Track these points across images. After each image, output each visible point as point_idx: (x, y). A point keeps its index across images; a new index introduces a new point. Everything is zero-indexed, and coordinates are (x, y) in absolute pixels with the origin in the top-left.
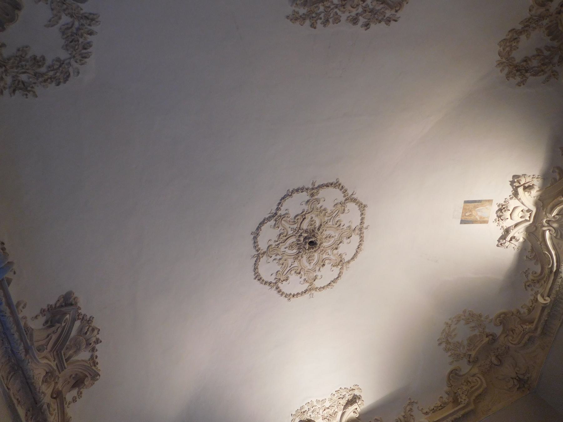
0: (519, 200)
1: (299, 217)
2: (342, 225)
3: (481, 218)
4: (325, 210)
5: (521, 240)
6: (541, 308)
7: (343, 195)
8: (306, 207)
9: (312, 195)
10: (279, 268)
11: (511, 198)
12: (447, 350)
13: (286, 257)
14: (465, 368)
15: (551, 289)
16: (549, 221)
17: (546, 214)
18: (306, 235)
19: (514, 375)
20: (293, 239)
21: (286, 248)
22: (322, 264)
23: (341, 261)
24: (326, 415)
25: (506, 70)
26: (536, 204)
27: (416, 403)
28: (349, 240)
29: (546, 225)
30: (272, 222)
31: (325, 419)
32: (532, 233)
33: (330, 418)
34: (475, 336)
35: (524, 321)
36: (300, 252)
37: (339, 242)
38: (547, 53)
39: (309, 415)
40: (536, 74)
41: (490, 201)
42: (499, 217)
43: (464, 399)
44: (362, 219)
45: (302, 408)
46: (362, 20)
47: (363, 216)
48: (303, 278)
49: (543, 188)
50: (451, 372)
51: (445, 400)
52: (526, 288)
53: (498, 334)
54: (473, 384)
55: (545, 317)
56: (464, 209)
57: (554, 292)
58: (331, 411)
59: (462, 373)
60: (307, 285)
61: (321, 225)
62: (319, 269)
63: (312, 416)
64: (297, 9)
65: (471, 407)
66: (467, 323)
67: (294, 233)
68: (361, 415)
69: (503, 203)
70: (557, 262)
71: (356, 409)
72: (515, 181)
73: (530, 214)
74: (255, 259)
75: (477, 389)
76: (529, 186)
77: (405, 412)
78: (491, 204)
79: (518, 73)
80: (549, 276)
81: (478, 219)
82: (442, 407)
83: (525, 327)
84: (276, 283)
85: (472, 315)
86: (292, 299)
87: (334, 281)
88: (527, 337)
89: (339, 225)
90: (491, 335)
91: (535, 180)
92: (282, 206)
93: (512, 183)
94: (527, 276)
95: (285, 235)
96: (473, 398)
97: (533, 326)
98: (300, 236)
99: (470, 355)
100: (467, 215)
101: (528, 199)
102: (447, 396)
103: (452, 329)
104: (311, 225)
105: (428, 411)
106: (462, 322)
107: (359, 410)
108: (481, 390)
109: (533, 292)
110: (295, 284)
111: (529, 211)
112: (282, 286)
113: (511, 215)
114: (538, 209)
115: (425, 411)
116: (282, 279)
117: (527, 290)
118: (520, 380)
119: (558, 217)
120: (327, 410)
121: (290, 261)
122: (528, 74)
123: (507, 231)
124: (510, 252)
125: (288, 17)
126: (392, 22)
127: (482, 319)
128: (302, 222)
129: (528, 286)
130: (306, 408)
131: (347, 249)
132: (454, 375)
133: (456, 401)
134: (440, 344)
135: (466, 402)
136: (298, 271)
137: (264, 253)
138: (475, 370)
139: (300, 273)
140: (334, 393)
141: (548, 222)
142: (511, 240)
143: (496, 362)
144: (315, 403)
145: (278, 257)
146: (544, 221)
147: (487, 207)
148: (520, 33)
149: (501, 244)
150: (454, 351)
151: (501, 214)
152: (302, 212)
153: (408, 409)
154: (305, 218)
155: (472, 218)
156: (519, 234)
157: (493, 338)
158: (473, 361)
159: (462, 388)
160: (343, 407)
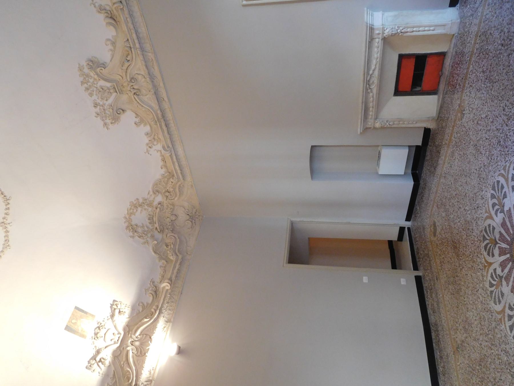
0: (113, 321)
3: (82, 330)
5: (107, 363)
7: (4, 216)
25: (126, 224)
26: (124, 330)
32: (117, 357)
38: (146, 229)
40: (140, 237)
41: (93, 316)
42: (96, 334)
46: (97, 110)
56: (73, 314)
64: (85, 66)
65: (180, 257)
72: (114, 305)
79: (131, 230)
81: (80, 331)
93: (112, 305)
101: (122, 320)
111: (119, 333)
123: (98, 352)
125: (79, 64)
142: (100, 361)
146: (129, 341)
148: (140, 205)
149: (90, 366)
156: (107, 355)
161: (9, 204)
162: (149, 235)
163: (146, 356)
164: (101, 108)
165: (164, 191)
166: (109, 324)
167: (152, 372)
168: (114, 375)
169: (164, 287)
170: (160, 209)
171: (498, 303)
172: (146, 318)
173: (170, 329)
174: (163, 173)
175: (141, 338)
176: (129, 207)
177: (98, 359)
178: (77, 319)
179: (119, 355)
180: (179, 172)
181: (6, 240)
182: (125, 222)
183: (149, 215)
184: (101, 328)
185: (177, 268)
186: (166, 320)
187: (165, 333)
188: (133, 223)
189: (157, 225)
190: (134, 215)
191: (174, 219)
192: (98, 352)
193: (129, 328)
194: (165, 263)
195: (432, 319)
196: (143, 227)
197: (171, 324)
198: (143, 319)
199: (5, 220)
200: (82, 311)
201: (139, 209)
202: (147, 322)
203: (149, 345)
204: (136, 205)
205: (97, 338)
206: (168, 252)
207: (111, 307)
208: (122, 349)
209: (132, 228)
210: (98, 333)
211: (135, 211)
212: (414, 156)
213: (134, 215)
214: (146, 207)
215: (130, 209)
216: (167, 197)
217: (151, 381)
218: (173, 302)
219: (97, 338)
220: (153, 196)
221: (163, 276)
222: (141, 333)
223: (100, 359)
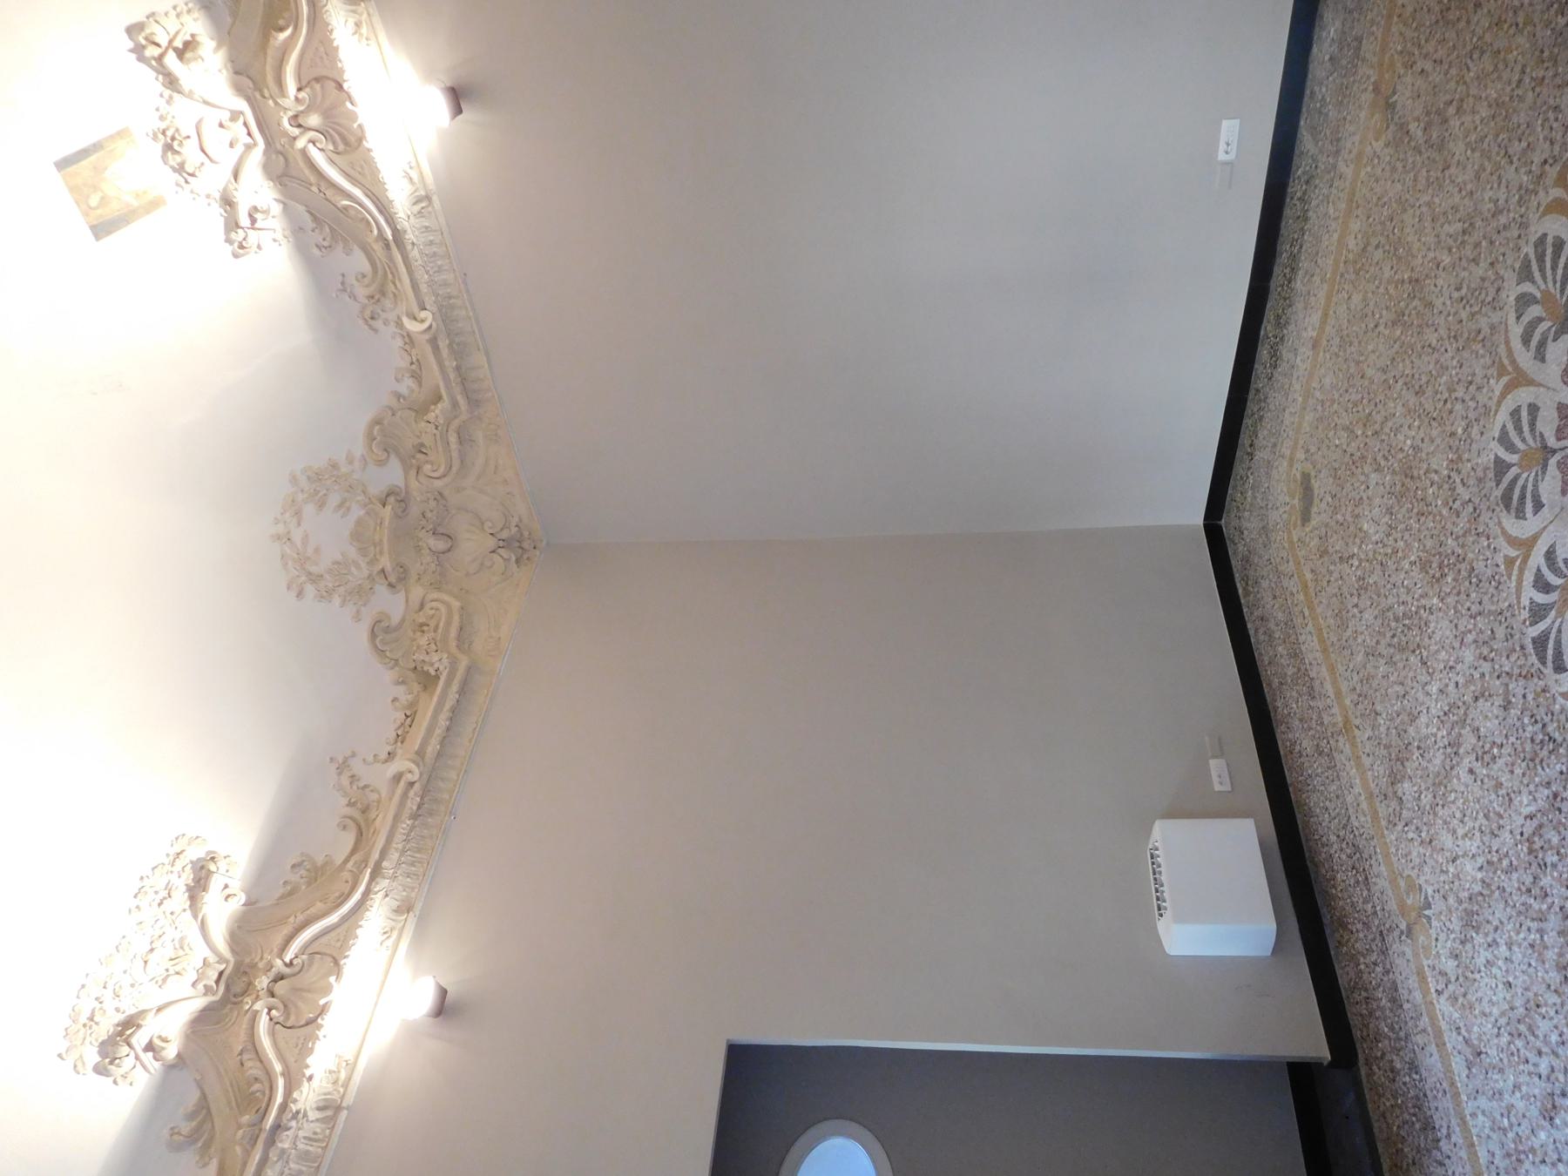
0: (190, 95)
11: (169, 101)
12: (326, 595)
14: (393, 605)
15: (415, 286)
16: (296, 116)
17: (276, 103)
19: (491, 543)
26: (239, 90)
27: (354, 755)
29: (296, 131)
31: (164, 980)
33: (177, 968)
34: (359, 522)
35: (421, 410)
41: (121, 134)
42: (180, 169)
43: (438, 662)
49: (227, 36)
50: (373, 635)
51: (405, 698)
52: (371, 327)
53: (401, 483)
54: (432, 624)
55: (450, 364)
56: (72, 189)
57: (424, 288)
58: (165, 952)
59: (395, 620)
65: (464, 662)
66: (321, 505)
68: (248, 892)
70: (381, 212)
71: (226, 886)
73: (245, 124)
75: (448, 623)
77: (345, 794)
80: (391, 258)
81: (135, 203)
82: (410, 717)
83: (431, 416)
85: (316, 477)
88: (453, 439)
91: (186, 18)
93: (138, 50)
94: (353, 296)
96: (453, 644)
97: (445, 404)
99: (383, 571)
101: (209, 72)
102: (402, 688)
103: (298, 543)
105: (389, 748)
106: (309, 509)
108: (456, 618)
109: (392, 328)
111: (235, 116)
114: (249, 100)
115: (384, 756)
117: (376, 331)
118: (506, 543)
119: (302, 95)
123: (228, 202)
124: (273, 267)
127: (344, 470)
132: (381, 633)
133: (428, 681)
134: (300, 595)
135: (445, 661)
138: (417, 592)
142: (253, 221)
143: (441, 545)
149: (241, 247)
150: (342, 589)
151: (178, 159)
153: (345, 781)
156: (257, 191)
157: (397, 498)
158: (398, 579)
159: (419, 647)
168: (315, 219)
171: (1550, 240)
172: (281, 29)
173: (376, 19)
175: (313, 98)
177: (244, 221)
178: (95, 188)
179: (286, 170)
184: (176, 147)
187: (373, 42)
192: (228, 202)
193: (252, 77)
195: (1306, 142)
200: (83, 154)
202: (292, 41)
205: (192, 175)
207: (142, 59)
212: (1295, 906)
217: (428, 198)
219: (192, 175)
222: (299, 78)
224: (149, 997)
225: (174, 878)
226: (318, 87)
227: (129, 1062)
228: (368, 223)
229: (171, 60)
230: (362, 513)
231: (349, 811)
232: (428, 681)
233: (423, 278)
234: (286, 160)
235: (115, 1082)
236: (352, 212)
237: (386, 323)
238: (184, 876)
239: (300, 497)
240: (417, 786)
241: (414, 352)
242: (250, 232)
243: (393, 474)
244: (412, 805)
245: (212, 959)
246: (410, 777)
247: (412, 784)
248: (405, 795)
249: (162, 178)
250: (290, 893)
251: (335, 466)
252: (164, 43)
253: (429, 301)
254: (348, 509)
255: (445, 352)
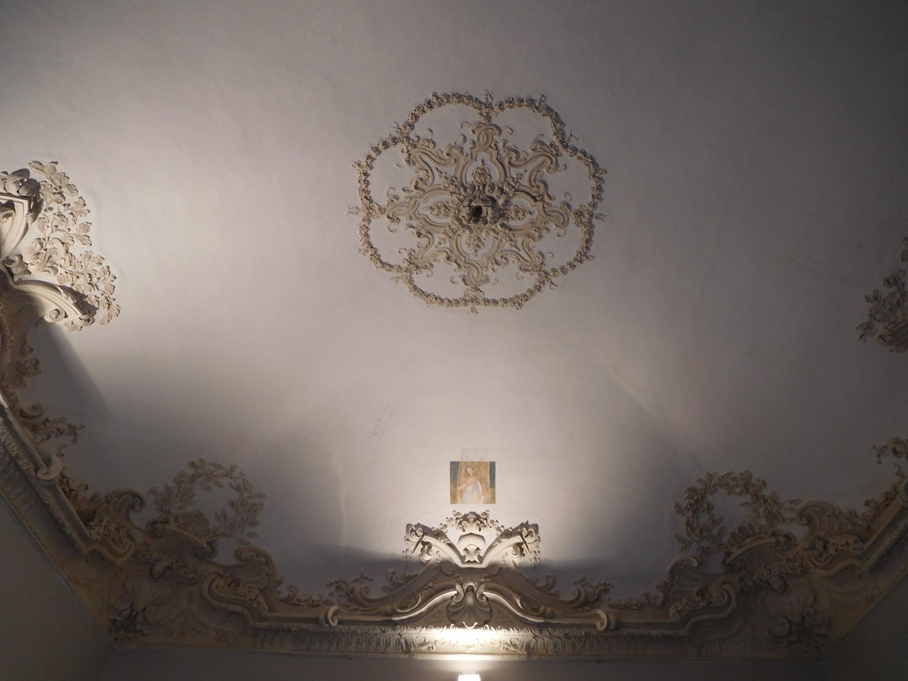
0: (498, 540)
1: (542, 190)
2: (495, 266)
3: (462, 491)
4: (540, 236)
5: (427, 558)
6: (312, 616)
7: (557, 267)
8: (557, 203)
9: (579, 214)
10: (443, 146)
11: (498, 529)
13: (462, 162)
14: (140, 519)
15: (357, 623)
18: (501, 202)
20: (496, 175)
21: (483, 162)
22: (423, 232)
23: (417, 267)
24: (49, 247)
25: (699, 486)
26: (492, 566)
27: (74, 441)
28: (460, 280)
29: (465, 588)
30: (550, 137)
31: (41, 244)
33: (41, 257)
36: (465, 189)
37: (462, 264)
38: (715, 531)
39: (52, 205)
40: (688, 524)
41: (493, 500)
42: (465, 518)
44: (495, 302)
45: (72, 188)
46: (886, 291)
47: (501, 303)
48: (402, 195)
50: (136, 495)
52: (332, 584)
55: (294, 626)
57: (353, 628)
58: (60, 258)
60: (384, 202)
61: (510, 229)
62: (412, 227)
63: (50, 214)
65: (84, 549)
66: (232, 504)
67: (510, 181)
69: (490, 518)
71: (66, 316)
72: (527, 529)
73: (475, 562)
74: (484, 100)
76: (522, 550)
78: (487, 503)
79: (692, 502)
80: (379, 614)
81: (459, 489)
84: (408, 138)
86: (356, 174)
87: (376, 257)
88: (237, 608)
89: (497, 263)
90: (212, 548)
91: (533, 555)
92: (579, 158)
93: (526, 525)
95: (514, 161)
98: (502, 191)
100: (469, 469)
101: (505, 554)
103: (220, 480)
104: (517, 212)
106: (235, 496)
107: (61, 322)
110: (394, 174)
111: (481, 559)
112: (398, 152)
113: (471, 534)
116: (413, 151)
117: (328, 586)
120: (62, 249)
121: (450, 170)
122: (690, 513)
124: (398, 545)
126: (860, 332)
128: (528, 194)
129: (338, 587)
130: (70, 199)
131: (442, 278)
132: (134, 500)
134: (193, 465)
135: (95, 537)
136: (421, 185)
137: (488, 118)
138: (140, 538)
139: (416, 187)
140: (105, 264)
141: (470, 590)
142: (424, 544)
144: (81, 220)
145: (467, 147)
146: (471, 584)
147: (483, 497)
148: (756, 496)
152: (549, 196)
153: (62, 426)
154: (536, 200)
155: (463, 478)
156: (439, 552)
157: (206, 554)
158: (154, 530)
160: (68, 285)
161: (581, 262)
162: (705, 544)
163: (448, 626)
164: (898, 296)
165: (821, 534)
166: (490, 534)
167: (425, 648)
168: (411, 578)
169: (598, 617)
170: (778, 543)
173: (513, 658)
174: (860, 514)
176: (737, 475)
177: (427, 539)
178: (475, 474)
179: (445, 573)
180: (881, 549)
181: (525, 296)
182: (700, 481)
183: (750, 525)
185: (653, 632)
186: (532, 645)
188: (710, 498)
189: (736, 552)
190: (729, 493)
191: (775, 586)
193: (497, 575)
194: (659, 602)
196: (715, 522)
197: (524, 658)
198: (519, 593)
199: (551, 274)
201: (747, 498)
202: (530, 606)
203: (470, 625)
204: (746, 485)
206: (684, 601)
207: (522, 525)
208: (457, 575)
209: (697, 500)
210: (468, 521)
211: (738, 490)
213: (729, 493)
214: (761, 510)
215: (734, 478)
216: (812, 547)
217: (408, 651)
218: (574, 647)
219: (460, 523)
220: (793, 515)
221: (627, 607)
223: (427, 543)
224: (35, 231)
225: (96, 292)
226: (488, 610)
227: (13, 189)
228: (406, 608)
229: (517, 539)
230: (211, 527)
231: (44, 417)
232: (88, 518)
233: (361, 629)
234: (448, 575)
235: (6, 173)
236: (413, 601)
237: (331, 594)
238: (93, 298)
239: (246, 494)
240: (33, 473)
241: (305, 605)
242: (418, 539)
243: (225, 556)
244: (24, 463)
245: (26, 277)
246: (43, 470)
247: (37, 469)
248: (32, 459)
249: (464, 509)
250: (22, 347)
251: (253, 524)
252: (526, 539)
253: (343, 628)
254: (219, 520)
255: (305, 626)
